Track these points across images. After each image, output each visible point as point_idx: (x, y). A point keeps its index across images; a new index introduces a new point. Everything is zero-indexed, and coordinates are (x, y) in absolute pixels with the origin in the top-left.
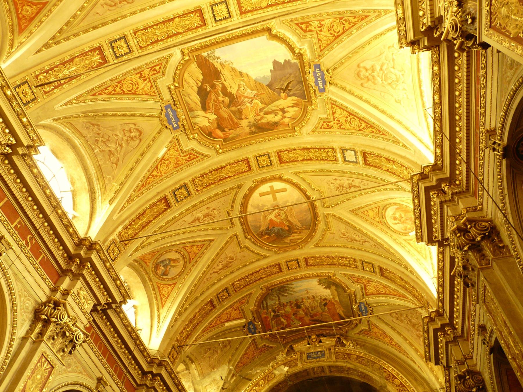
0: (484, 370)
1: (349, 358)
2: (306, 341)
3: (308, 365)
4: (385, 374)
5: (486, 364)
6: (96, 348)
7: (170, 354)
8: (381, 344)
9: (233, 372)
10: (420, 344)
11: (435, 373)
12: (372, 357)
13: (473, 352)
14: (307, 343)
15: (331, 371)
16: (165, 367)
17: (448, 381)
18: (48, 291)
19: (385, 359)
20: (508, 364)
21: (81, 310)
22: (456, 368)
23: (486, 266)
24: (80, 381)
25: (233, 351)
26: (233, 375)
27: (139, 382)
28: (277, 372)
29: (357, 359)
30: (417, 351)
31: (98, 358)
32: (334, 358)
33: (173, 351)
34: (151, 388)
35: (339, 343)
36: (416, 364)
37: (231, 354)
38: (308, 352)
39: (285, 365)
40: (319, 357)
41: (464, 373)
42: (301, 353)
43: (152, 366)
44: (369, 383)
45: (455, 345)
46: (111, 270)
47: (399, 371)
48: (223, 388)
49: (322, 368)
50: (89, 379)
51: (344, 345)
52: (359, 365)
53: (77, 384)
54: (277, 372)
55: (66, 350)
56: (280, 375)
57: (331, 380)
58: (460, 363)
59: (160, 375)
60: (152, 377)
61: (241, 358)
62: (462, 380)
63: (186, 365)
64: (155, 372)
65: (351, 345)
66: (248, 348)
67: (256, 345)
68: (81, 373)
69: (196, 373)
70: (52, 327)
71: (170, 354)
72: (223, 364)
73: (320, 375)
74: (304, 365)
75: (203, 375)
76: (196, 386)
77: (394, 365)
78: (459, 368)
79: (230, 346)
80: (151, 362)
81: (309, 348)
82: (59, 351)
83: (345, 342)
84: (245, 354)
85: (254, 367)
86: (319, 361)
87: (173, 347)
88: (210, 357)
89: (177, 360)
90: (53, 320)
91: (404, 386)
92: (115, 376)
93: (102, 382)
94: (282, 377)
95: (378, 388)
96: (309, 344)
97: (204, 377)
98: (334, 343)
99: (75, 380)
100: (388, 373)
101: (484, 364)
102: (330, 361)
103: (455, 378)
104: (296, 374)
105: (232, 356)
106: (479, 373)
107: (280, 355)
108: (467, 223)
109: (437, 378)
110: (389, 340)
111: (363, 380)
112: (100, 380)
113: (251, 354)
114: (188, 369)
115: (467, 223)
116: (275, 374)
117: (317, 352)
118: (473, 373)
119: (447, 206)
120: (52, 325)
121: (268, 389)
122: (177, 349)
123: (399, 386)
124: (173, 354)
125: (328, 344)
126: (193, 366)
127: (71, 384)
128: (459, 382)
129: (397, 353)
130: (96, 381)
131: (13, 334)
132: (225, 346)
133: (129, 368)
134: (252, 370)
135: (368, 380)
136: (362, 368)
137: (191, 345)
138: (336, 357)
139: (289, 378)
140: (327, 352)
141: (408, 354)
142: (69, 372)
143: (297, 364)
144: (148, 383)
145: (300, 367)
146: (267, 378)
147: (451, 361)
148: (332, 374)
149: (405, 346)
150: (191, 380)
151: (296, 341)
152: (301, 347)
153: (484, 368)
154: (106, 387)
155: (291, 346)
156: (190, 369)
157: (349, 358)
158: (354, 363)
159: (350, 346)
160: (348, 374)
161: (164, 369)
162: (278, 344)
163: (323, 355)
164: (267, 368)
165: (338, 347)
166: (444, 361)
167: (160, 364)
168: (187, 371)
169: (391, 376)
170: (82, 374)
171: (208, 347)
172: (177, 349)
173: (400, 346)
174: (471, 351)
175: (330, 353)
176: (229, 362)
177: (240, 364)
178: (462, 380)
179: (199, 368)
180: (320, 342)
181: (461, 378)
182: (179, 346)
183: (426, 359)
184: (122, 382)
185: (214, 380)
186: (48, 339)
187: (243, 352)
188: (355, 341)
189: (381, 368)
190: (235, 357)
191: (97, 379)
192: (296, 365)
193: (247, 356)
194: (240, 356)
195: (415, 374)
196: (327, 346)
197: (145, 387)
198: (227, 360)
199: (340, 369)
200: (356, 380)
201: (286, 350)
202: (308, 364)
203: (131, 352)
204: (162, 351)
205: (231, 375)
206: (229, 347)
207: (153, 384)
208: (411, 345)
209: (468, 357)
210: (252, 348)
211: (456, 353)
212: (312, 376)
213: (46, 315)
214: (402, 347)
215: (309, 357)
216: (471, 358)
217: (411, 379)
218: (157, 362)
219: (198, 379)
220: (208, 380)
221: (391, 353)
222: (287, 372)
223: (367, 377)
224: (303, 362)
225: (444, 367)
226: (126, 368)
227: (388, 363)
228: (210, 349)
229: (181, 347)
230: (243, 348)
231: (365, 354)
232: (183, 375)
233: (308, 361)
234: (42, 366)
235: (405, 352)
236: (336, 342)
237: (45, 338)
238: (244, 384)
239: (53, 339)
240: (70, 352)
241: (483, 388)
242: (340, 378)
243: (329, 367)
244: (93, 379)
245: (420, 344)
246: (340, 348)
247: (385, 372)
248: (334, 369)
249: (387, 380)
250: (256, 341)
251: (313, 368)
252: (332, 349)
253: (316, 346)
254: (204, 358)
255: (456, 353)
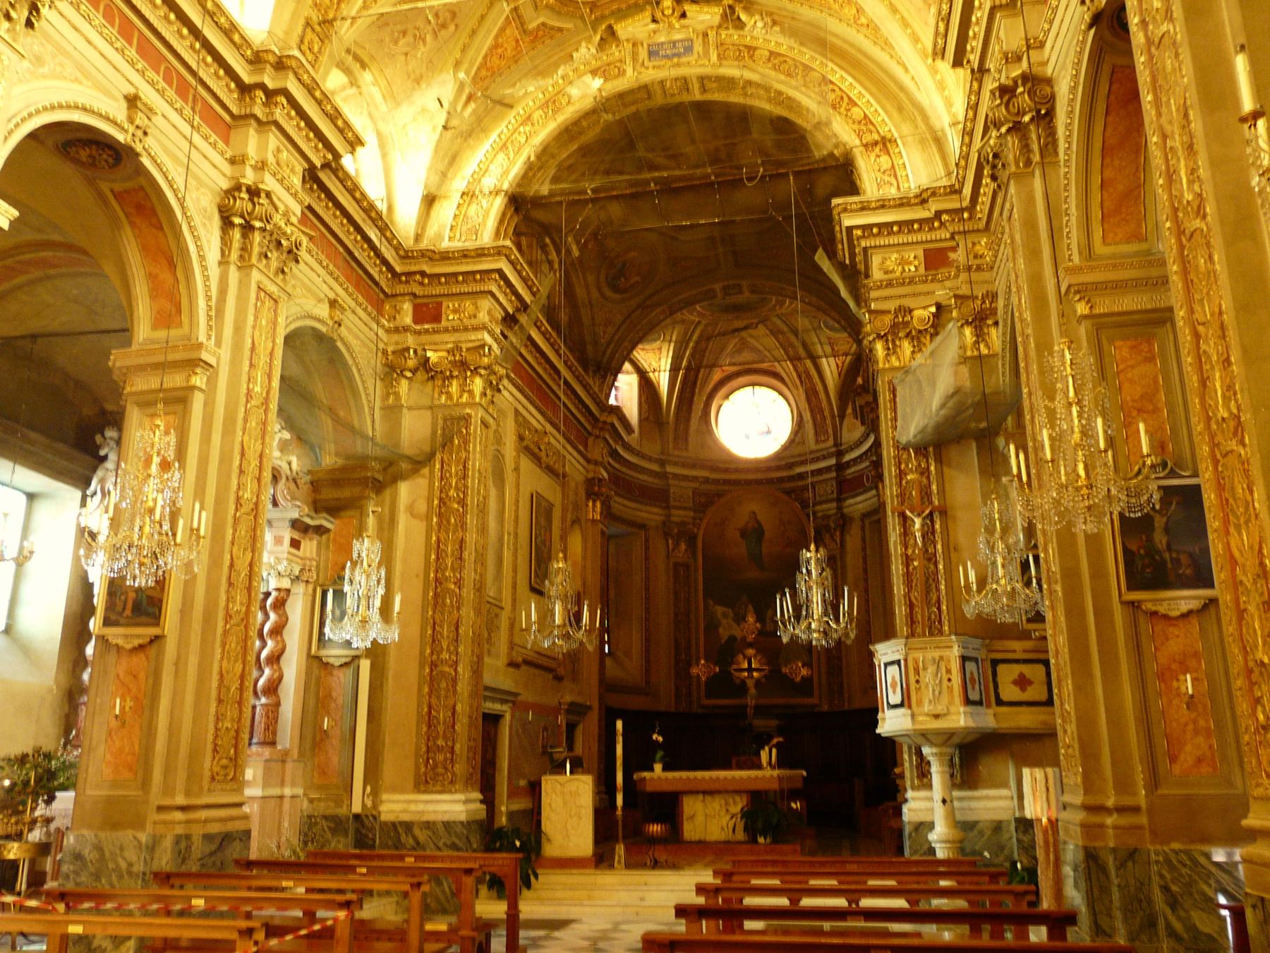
0: (1063, 73)
1: (751, 57)
2: (647, 14)
3: (652, 73)
4: (831, 96)
5: (1072, 53)
6: (99, 19)
7: (302, 41)
8: (833, 25)
9: (467, 91)
10: (926, 23)
11: (946, 93)
12: (806, 55)
13: (1049, 30)
14: (649, 20)
15: (704, 89)
16: (296, 74)
17: (973, 107)
18: (227, 168)
19: (837, 60)
20: (1129, 53)
21: (288, 189)
22: (1000, 72)
23: (1023, 176)
24: (81, 101)
25: (464, 38)
26: (470, 98)
27: (235, 110)
28: (574, 92)
29: (769, 60)
30: (916, 39)
31: (112, 44)
32: (714, 58)
33: (310, 35)
34: (268, 123)
35: (730, 18)
36: (907, 70)
37: (460, 46)
38: (650, 42)
39: (594, 73)
40: (679, 55)
41: (1016, 82)
42: (634, 45)
43: (262, 71)
44: (791, 116)
45: (1014, 15)
46: (301, 71)
47: (866, 88)
48: (445, 127)
49: (685, 82)
50: (100, 96)
51: (740, 25)
52: (773, 73)
53: (77, 107)
54: (574, 92)
55: (13, 14)
56: (583, 97)
57: (704, 110)
58: (1012, 58)
59: (285, 92)
60: (267, 98)
61: (485, 57)
62: (1006, 98)
63: (347, 71)
64: (271, 85)
65: (760, 24)
66: (502, 30)
67: (522, 24)
68: (76, 80)
69: (376, 93)
70: (257, 237)
71: (302, 41)
72: (441, 70)
73: (678, 99)
74: (640, 73)
75: (393, 98)
76: (382, 126)
77: (853, 72)
78: (1007, 70)
79: (456, 26)
80: (257, 60)
81: (655, 32)
82: (276, 274)
83: (743, 17)
84: (496, 46)
85: (520, 80)
86: (678, 65)
87: (308, 24)
88: (406, 54)
89: (324, 59)
90: (257, 224)
91: (872, 123)
92: (170, 93)
93: (139, 104)
94: (588, 104)
95: (808, 127)
96: (654, 21)
97: (398, 105)
98: (717, 20)
99: (64, 98)
100: (839, 93)
101: (1066, 56)
102: (703, 65)
103: (992, 92)
104: (621, 96)
105: (464, 49)
106: (1049, 81)
107: (583, 50)
108: (1020, 82)
109: (949, 103)
110: (854, 11)
111: (779, 111)
112: (133, 101)
113: (510, 46)
114: (354, 83)
115: (1020, 82)
116: (570, 97)
117: (674, 43)
118: (1036, 82)
119: (1002, 17)
120: (257, 234)
121: (553, 131)
122: (317, 28)
123: (860, 122)
124: (311, 42)
125: (703, 21)
126: (366, 77)
127: (61, 107)
128: (998, 101)
129: (867, 45)
130: (124, 104)
131: (202, 258)
132: (444, 26)
133: (202, 74)
134: (514, 85)
135: (790, 108)
136: (780, 83)
137: (354, 18)
138: (719, 55)
139: (603, 105)
140: (698, 47)
141: (891, 47)
142: (45, 77)
143: (624, 71)
144: (258, 111)
145: (629, 78)
146: (551, 104)
147: (993, 54)
148: (709, 97)
149: (890, 27)
150: (365, 112)
151: (622, 14)
152: (635, 28)
153: (1064, 66)
154: (154, 118)
155: (610, 27)
156: (361, 83)
157: (751, 57)
158: (760, 70)
159: (755, 28)
160: (745, 95)
161: (291, 76)
162: (579, 22)
163: (689, 49)
164: (551, 81)
165: (727, 28)
166: (974, 58)
167: (281, 65)
168: (354, 90)
169: (846, 100)
170: (81, 83)
171: (399, 27)
172: (317, 28)
173: (877, 29)
174: (1046, 26)
175: (705, 43)
176: (457, 65)
177: (484, 73)
178: (1006, 98)
179: (383, 83)
180: (684, 15)
181: (1006, 92)
182: (324, 22)
183: (935, 54)
184: (193, 109)
185: (424, 110)
186: (259, 260)
187: (489, 42)
188: (770, 14)
189: (825, 81)
190: (471, 53)
191: (126, 97)
192: (622, 73)
193: (500, 51)
194: (483, 53)
195: (902, 95)
196: (701, 28)
197: (252, 121)
198: (451, 61)
199: (728, 83)
200: (763, 110)
201: (598, 37)
202: (651, 71)
203: (195, 32)
204: (280, 34)
205: (464, 97)
206: (452, 28)
207: (272, 114)
208: (905, 24)
209: (1035, 44)
210: (513, 31)
211: (1009, 34)
212: (659, 100)
213: (242, 216)
214: (884, 30)
215: (651, 54)
216: (1042, 45)
217: (889, 107)
218: (271, 58)
219: (384, 108)
220: (406, 112)
221: (852, 45)
222: (600, 90)
223: (790, 103)
224: (638, 67)
225: (973, 71)
226: (194, 73)
227: (842, 68)
228: (404, 33)
229: (327, 22)
230: (489, 32)
231: (791, 48)
232: (345, 100)
233: (651, 64)
234: (263, 303)
235: (886, 42)
236: (724, 16)
237: (254, 260)
238: (498, 118)
239: (266, 256)
240: (29, 24)
241: (1046, 114)
242: (726, 105)
243: (702, 79)
244: (115, 99)
245: (926, 23)
246: (731, 31)
247: (833, 91)
248: (714, 85)
249: (834, 107)
250: (522, 11)
251: (662, 82)
252: (712, 34)
253: (671, 26)
254: (392, 56)
255: (1009, 34)
